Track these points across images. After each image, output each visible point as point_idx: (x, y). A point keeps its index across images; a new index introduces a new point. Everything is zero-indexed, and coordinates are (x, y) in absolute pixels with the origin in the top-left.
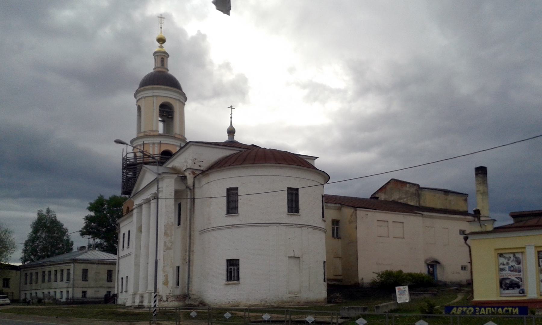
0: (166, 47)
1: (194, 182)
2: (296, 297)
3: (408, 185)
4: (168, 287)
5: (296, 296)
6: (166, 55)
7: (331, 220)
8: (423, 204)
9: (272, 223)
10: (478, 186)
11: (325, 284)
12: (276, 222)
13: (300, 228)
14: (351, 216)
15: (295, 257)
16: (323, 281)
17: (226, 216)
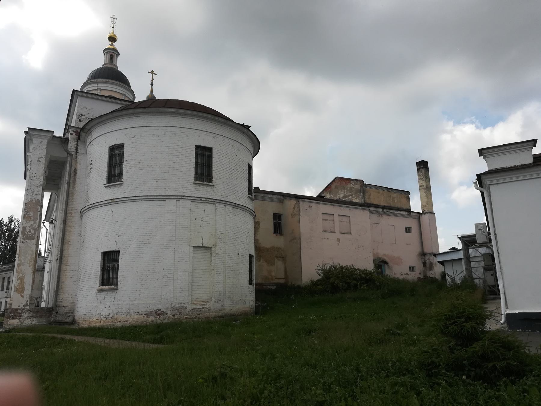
0: (116, 45)
1: (77, 145)
2: (203, 308)
3: (352, 182)
4: (22, 296)
5: (204, 307)
7: (272, 214)
8: (368, 201)
9: (170, 196)
10: (420, 181)
11: (252, 288)
13: (214, 205)
14: (294, 208)
15: (205, 247)
16: (247, 282)
17: (106, 187)
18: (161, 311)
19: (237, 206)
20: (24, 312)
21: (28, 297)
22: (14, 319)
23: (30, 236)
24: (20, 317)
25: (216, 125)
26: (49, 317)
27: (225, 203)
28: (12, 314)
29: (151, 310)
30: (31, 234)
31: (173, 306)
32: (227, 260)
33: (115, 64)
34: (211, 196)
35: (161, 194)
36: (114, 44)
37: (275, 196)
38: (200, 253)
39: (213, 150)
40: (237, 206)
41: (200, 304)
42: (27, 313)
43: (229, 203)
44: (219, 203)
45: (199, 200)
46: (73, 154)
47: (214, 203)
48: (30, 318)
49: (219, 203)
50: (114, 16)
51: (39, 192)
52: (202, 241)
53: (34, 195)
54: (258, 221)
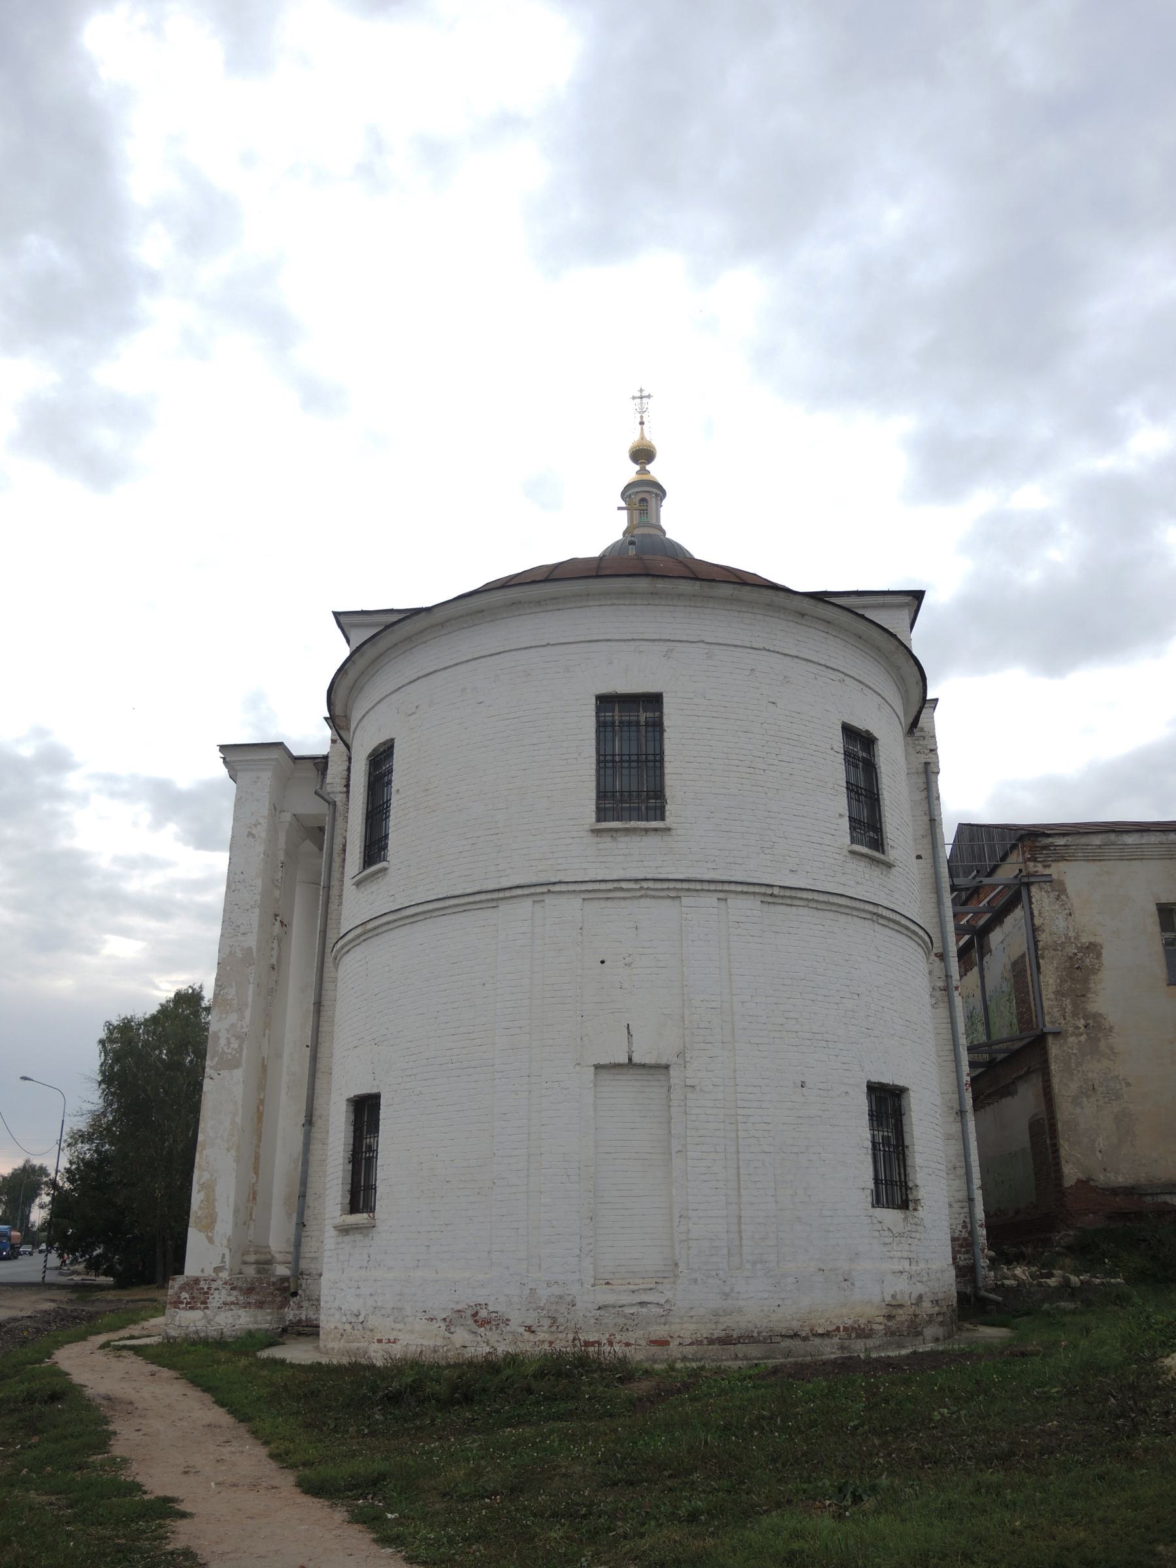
0: (656, 470)
4: (211, 1240)
5: (645, 1298)
6: (658, 492)
7: (1154, 909)
12: (535, 880)
13: (677, 902)
18: (491, 1308)
19: (783, 897)
20: (215, 1289)
21: (225, 1242)
22: (190, 1308)
23: (230, 1057)
24: (204, 1303)
25: (671, 608)
26: (282, 1307)
27: (722, 888)
28: (184, 1295)
29: (459, 1307)
30: (230, 1051)
31: (527, 1292)
32: (740, 1111)
33: (654, 521)
34: (660, 870)
35: (484, 888)
36: (648, 467)
37: (1153, 838)
38: (624, 1090)
39: (664, 700)
40: (783, 897)
41: (631, 1287)
42: (224, 1292)
43: (739, 888)
44: (697, 890)
45: (610, 890)
46: (339, 799)
47: (672, 894)
48: (232, 1307)
49: (695, 894)
50: (641, 391)
51: (251, 925)
52: (630, 1043)
53: (239, 934)
54: (1093, 940)
